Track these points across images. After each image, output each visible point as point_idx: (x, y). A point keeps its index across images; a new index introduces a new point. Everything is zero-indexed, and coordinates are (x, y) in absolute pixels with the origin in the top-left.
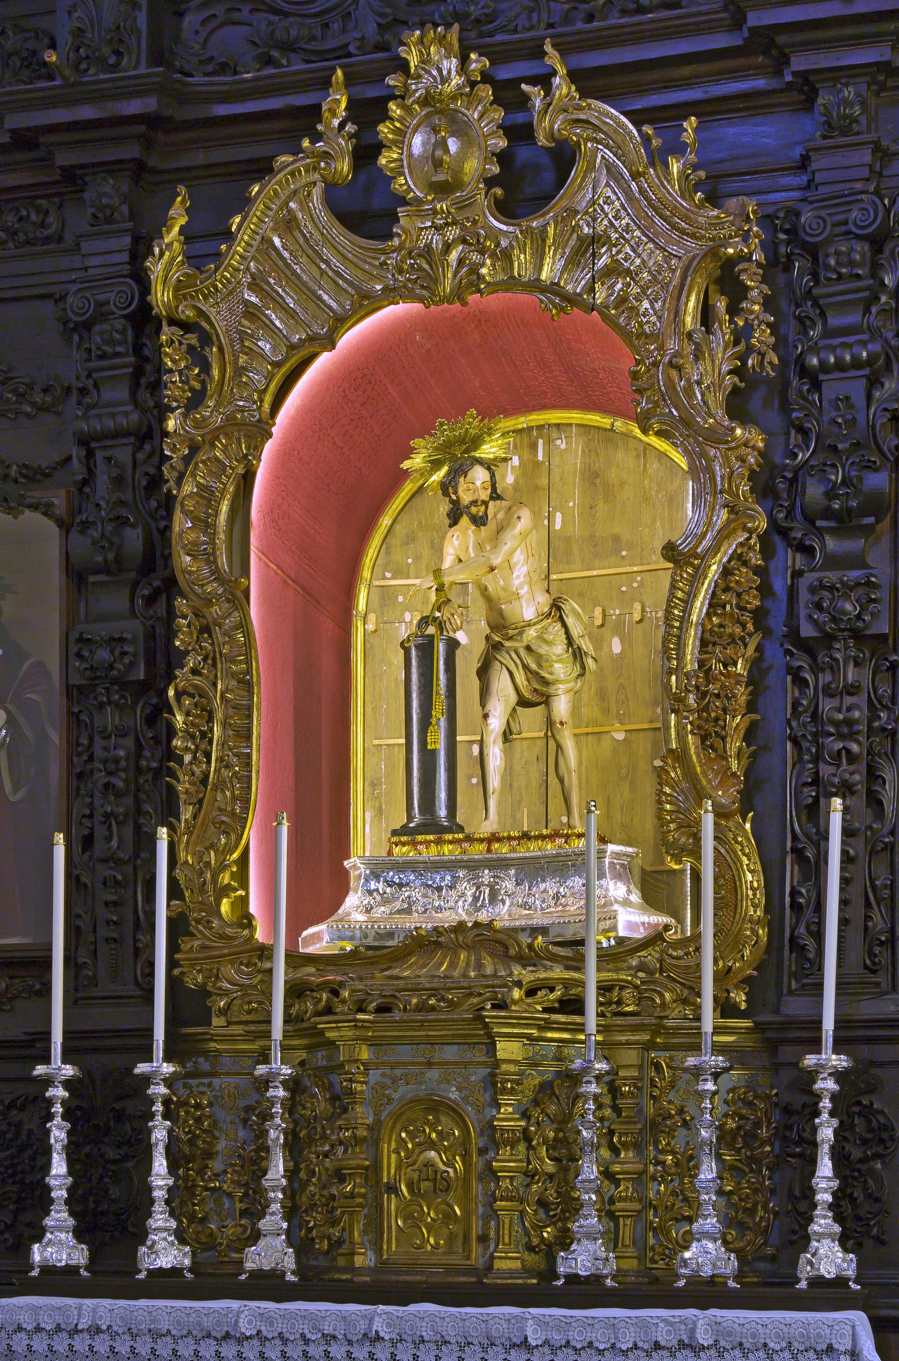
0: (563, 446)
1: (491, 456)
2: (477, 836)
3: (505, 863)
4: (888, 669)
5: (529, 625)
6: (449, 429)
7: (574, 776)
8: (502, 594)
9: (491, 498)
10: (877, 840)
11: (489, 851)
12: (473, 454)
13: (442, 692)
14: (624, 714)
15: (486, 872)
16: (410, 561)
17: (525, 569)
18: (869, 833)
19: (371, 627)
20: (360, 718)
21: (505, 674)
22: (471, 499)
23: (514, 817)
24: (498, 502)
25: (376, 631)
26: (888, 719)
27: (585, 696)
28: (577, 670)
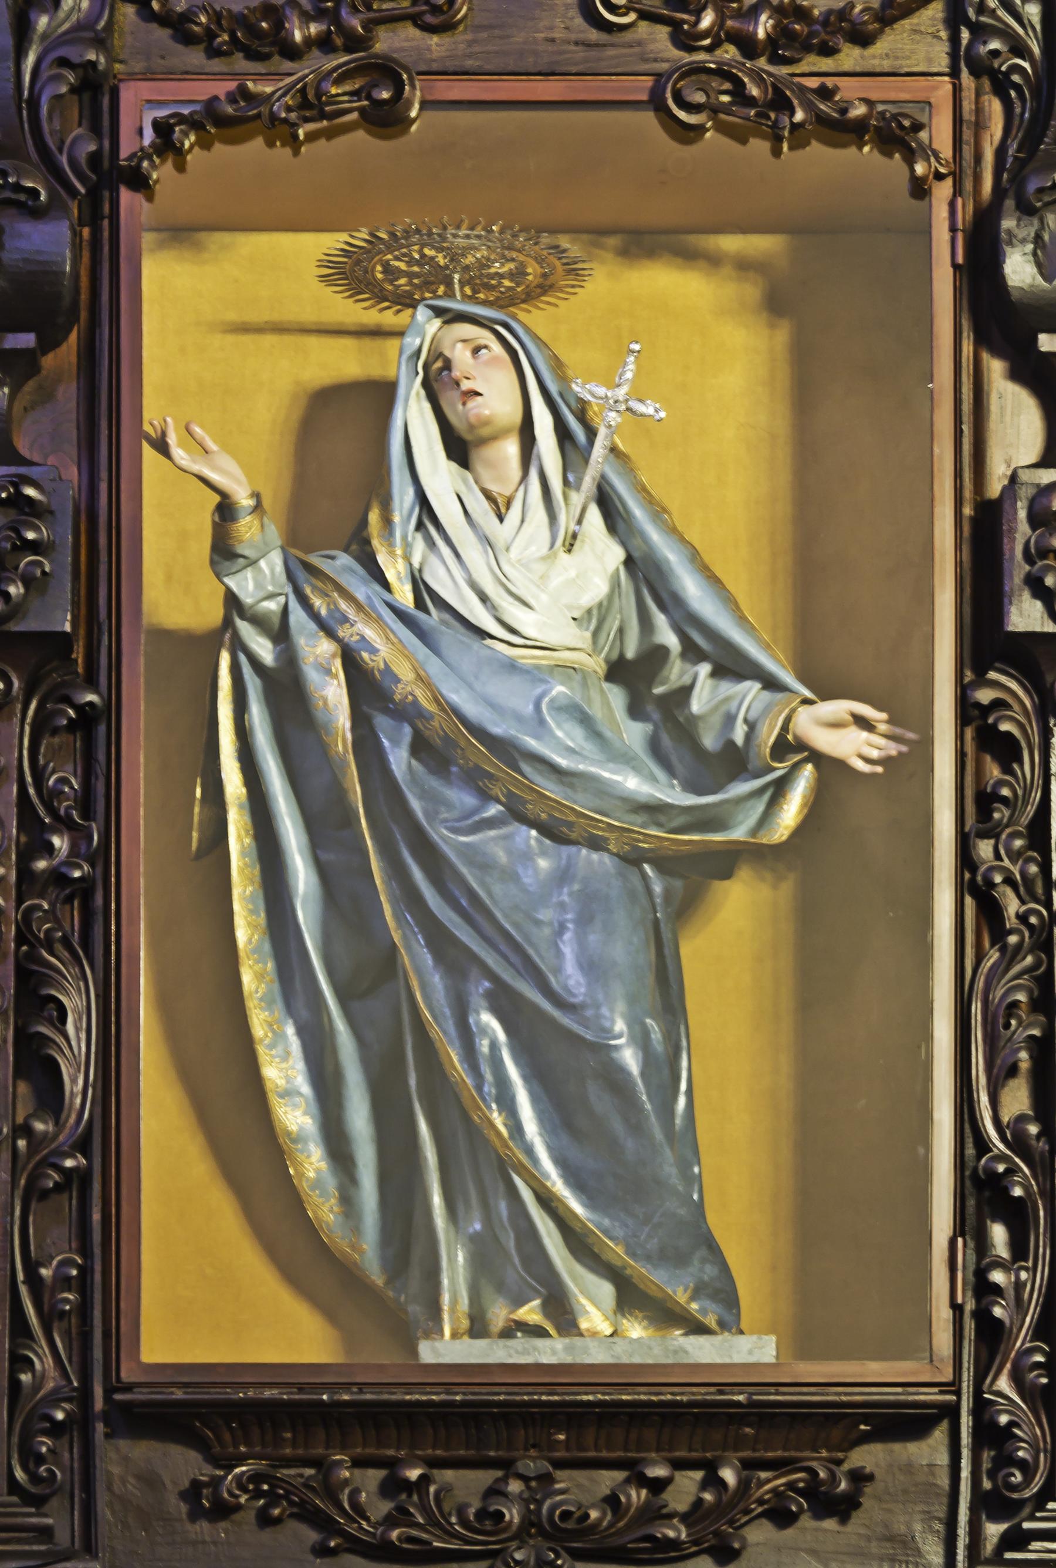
4: (72, 726)
10: (46, 1163)
18: (22, 1143)
26: (74, 851)
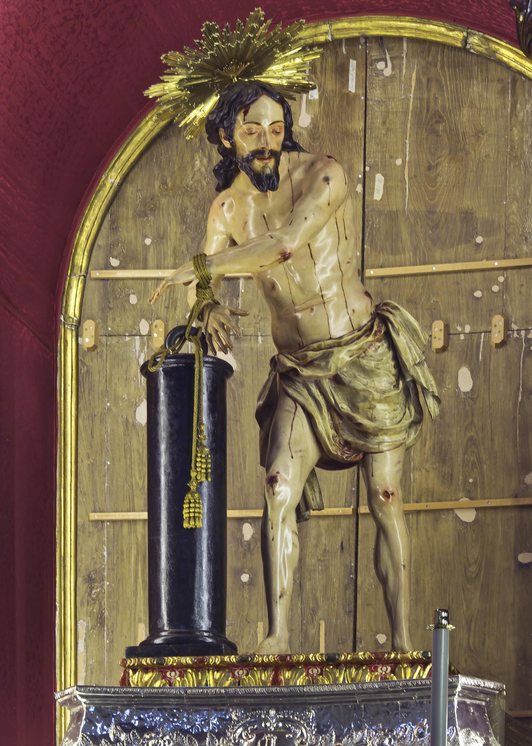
0: (388, 72)
1: (284, 82)
2: (258, 659)
3: (299, 700)
5: (339, 343)
6: (221, 38)
7: (403, 574)
8: (298, 296)
9: (285, 148)
11: (276, 682)
12: (257, 78)
13: (205, 442)
14: (475, 484)
15: (272, 712)
16: (148, 241)
17: (333, 259)
19: (87, 341)
20: (70, 479)
21: (301, 419)
22: (253, 148)
23: (306, 636)
24: (294, 155)
25: (95, 347)
27: (415, 455)
28: (410, 415)
